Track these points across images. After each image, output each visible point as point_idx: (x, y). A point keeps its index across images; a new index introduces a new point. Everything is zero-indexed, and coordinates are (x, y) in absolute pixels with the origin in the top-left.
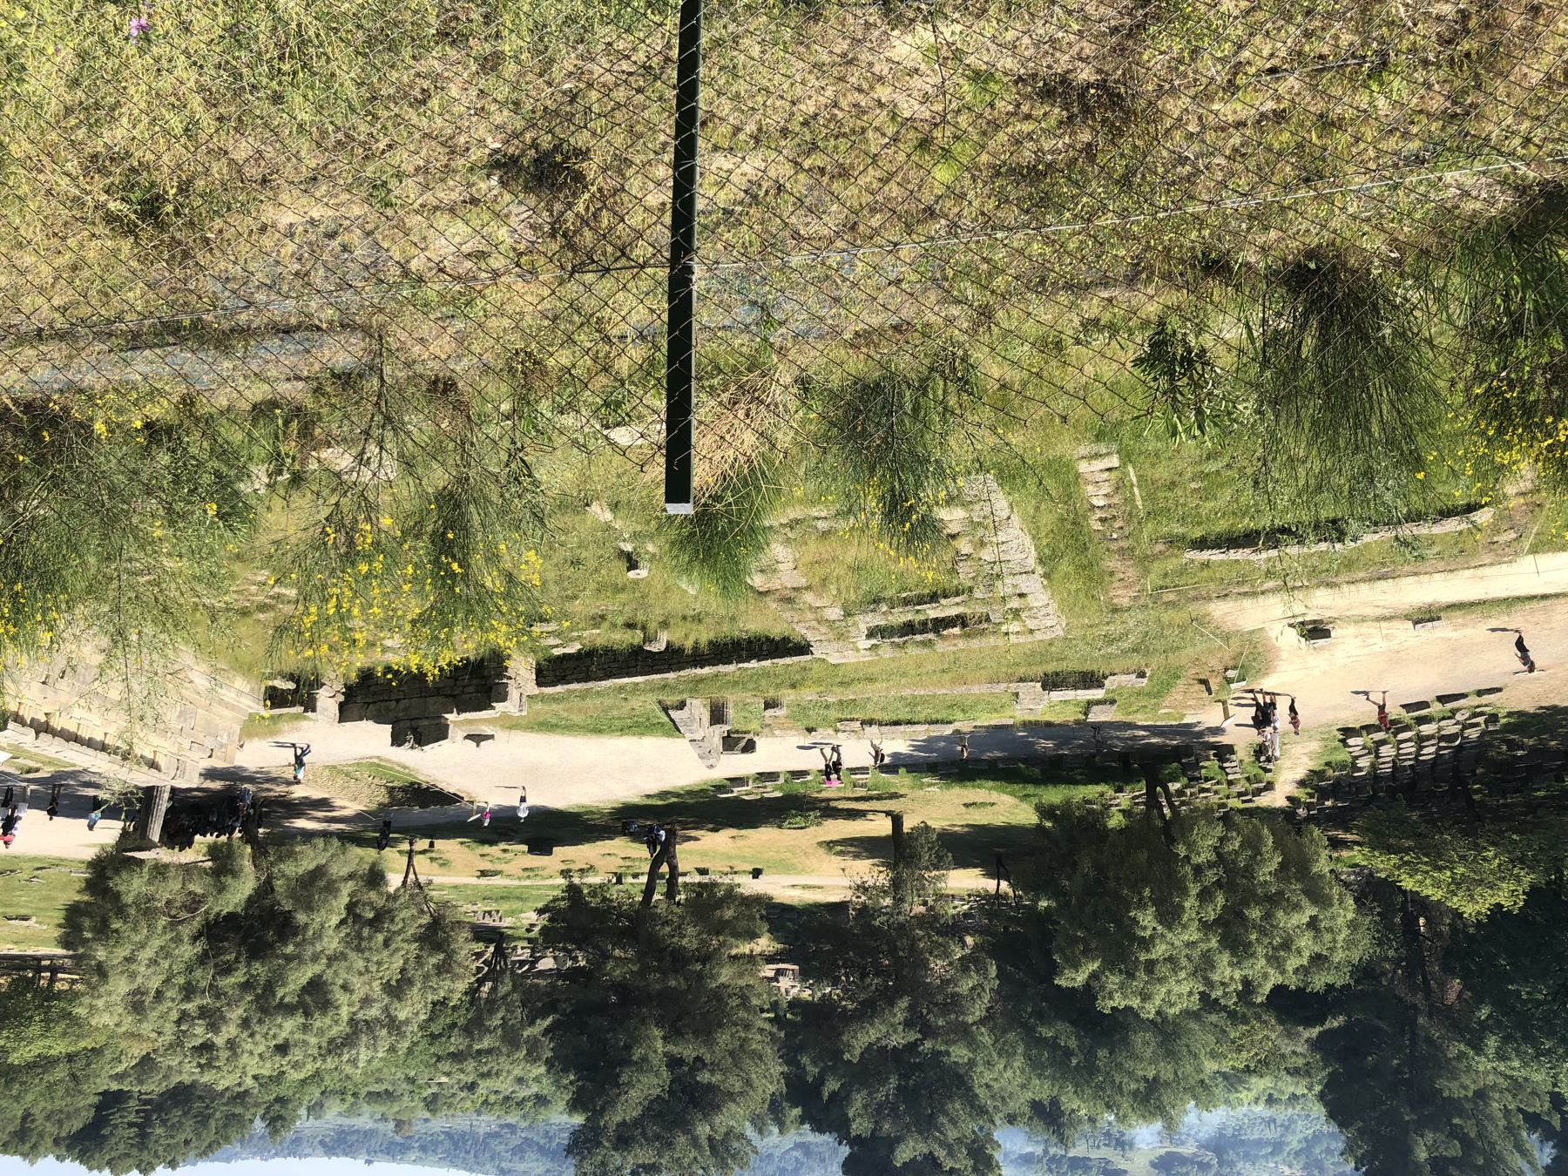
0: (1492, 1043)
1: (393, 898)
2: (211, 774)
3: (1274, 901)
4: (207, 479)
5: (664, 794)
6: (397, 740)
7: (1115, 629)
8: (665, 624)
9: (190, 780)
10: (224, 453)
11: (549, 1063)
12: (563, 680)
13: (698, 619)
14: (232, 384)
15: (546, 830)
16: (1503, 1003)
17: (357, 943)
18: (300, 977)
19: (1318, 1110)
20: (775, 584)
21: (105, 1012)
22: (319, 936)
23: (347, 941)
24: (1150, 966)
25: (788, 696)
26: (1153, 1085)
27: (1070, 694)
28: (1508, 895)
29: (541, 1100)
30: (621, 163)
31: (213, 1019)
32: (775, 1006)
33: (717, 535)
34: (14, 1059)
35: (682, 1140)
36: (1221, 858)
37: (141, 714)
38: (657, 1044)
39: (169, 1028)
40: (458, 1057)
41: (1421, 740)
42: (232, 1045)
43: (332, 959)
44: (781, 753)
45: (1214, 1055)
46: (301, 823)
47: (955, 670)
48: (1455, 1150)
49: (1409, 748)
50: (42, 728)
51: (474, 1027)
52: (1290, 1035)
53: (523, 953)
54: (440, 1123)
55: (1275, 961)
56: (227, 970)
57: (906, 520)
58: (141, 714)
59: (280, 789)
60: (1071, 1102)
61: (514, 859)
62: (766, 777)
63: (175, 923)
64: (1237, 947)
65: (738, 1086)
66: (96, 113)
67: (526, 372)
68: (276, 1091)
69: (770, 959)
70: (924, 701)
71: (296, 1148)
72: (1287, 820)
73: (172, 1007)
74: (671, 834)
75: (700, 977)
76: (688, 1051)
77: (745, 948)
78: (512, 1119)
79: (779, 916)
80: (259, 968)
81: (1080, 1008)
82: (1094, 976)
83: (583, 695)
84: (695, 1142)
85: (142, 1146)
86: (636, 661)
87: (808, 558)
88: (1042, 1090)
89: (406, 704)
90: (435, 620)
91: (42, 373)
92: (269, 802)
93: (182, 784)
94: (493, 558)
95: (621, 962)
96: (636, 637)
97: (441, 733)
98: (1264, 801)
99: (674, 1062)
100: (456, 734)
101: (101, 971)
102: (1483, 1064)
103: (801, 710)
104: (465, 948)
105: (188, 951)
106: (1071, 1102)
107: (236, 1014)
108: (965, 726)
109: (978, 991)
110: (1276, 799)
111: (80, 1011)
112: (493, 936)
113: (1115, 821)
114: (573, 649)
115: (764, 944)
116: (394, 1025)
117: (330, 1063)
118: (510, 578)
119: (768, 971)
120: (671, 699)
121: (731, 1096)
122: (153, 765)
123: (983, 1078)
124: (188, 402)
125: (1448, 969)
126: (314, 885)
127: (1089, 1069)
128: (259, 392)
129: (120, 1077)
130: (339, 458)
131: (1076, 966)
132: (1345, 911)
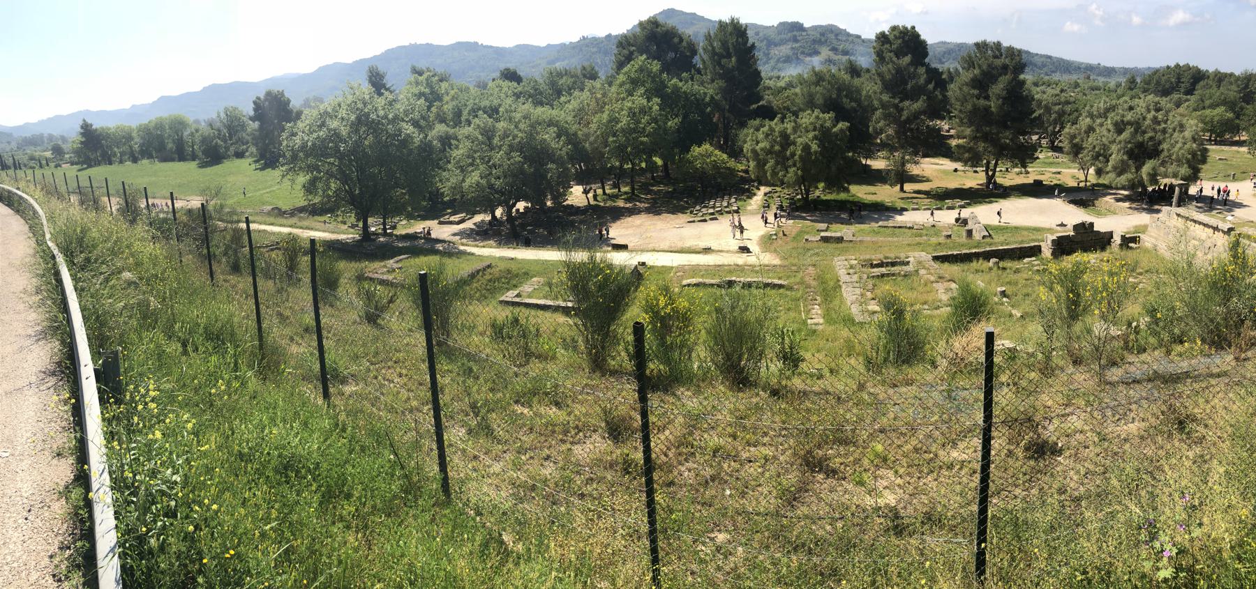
0: (708, 99)
1: (1092, 164)
2: (1158, 211)
3: (769, 152)
4: (1161, 324)
5: (991, 202)
6: (1092, 225)
7: (815, 258)
8: (991, 269)
9: (1165, 209)
10: (1155, 334)
11: (1033, 99)
12: (1031, 248)
13: (977, 271)
14: (1153, 361)
15: (1038, 190)
16: (702, 113)
17: (1105, 147)
18: (1125, 135)
19: (763, 74)
20: (946, 284)
21: (1193, 124)
22: (1119, 150)
23: (1109, 148)
24: (815, 130)
25: (942, 240)
26: (817, 83)
27: (833, 235)
28: (696, 150)
29: (1036, 84)
30: (1010, 454)
31: (1156, 121)
32: (950, 118)
33: (971, 308)
34: (1223, 108)
35: (985, 67)
36: (786, 169)
37: (1183, 235)
38: (994, 105)
39: (1171, 118)
40: (1068, 103)
41: (714, 207)
42: (1149, 111)
43: (1114, 141)
44: (946, 217)
45: (796, 94)
46: (1126, 193)
47: (877, 247)
48: (724, 61)
49: (718, 204)
50: (1216, 229)
51: (1062, 114)
52: (769, 102)
53: (1044, 142)
54: (1074, 77)
55: (772, 130)
56: (1151, 138)
57: (895, 309)
58: (1183, 235)
59: (1134, 206)
60: (846, 77)
61: (1048, 179)
62: (952, 208)
63: (1170, 156)
64: (784, 135)
65: (965, 88)
66: (1201, 460)
67: (1047, 370)
68: (1133, 93)
69: (951, 136)
70: (889, 235)
71: (1125, 71)
72: (761, 182)
73: (1170, 126)
74: (988, 186)
75: (977, 131)
76: (982, 102)
77: (961, 141)
78: (1047, 78)
79: (948, 153)
80: (1140, 139)
81: (841, 113)
82: (835, 126)
83: (1022, 242)
84: (980, 66)
85: (1179, 74)
86: (1002, 255)
87: (936, 293)
88: (857, 81)
89: (1088, 239)
90: (1079, 271)
91: (1218, 361)
92: (1138, 201)
93: (1168, 208)
94: (1058, 297)
95: (1006, 138)
96: (1001, 264)
97: (1076, 227)
98: (768, 189)
99: (987, 98)
100: (1070, 227)
101: (1194, 140)
102: (711, 92)
103: (936, 235)
104: (1065, 145)
105: (1165, 146)
106: (846, 77)
107: (1148, 122)
108: (874, 225)
109: (877, 122)
110: (764, 189)
111: (1201, 125)
112: (1055, 149)
113: (821, 185)
114: (1027, 260)
115: (954, 142)
116: (1091, 116)
117: (1114, 102)
118: (1051, 289)
119: (952, 132)
120: (988, 240)
121: (967, 84)
122: (1178, 215)
123: (878, 87)
124: (1168, 353)
125: (716, 125)
126: (1120, 170)
127: (839, 90)
128: (1144, 357)
129: (1187, 100)
130: (1115, 331)
131: (841, 130)
132: (747, 147)
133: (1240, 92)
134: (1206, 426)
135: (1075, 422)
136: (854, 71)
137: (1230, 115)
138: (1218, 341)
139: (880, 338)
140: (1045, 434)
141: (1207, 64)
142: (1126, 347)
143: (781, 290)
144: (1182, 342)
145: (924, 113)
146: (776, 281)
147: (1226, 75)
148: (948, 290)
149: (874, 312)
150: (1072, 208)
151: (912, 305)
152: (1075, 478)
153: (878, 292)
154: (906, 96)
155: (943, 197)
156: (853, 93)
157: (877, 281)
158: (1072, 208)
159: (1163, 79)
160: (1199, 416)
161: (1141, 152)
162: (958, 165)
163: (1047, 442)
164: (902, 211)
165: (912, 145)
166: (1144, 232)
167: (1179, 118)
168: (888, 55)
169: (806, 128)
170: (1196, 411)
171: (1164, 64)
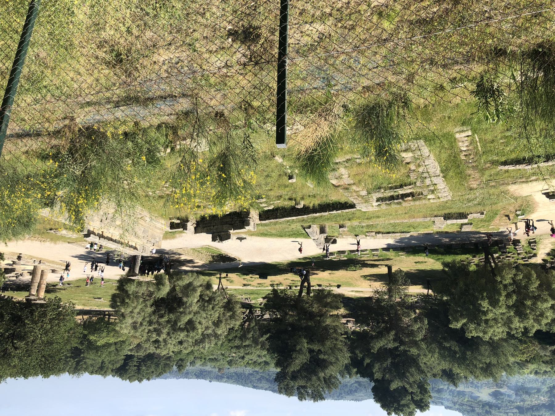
1: (215, 293)
3: (536, 298)
6: (214, 239)
7: (471, 196)
8: (302, 198)
9: (147, 254)
12: (268, 218)
13: (314, 196)
15: (264, 270)
21: (125, 329)
22: (191, 305)
23: (200, 307)
24: (486, 321)
25: (348, 223)
27: (455, 221)
29: (266, 363)
31: (158, 332)
33: (315, 162)
34: (99, 344)
35: (314, 378)
36: (514, 282)
39: (145, 335)
40: (238, 347)
42: (165, 341)
43: (195, 313)
44: (344, 244)
45: (513, 355)
46: (184, 268)
47: (409, 213)
50: (101, 236)
51: (243, 337)
52: (545, 349)
53: (258, 313)
54: (233, 370)
56: (162, 316)
57: (386, 156)
59: (177, 257)
61: (255, 280)
64: (521, 314)
65: (333, 360)
69: (344, 317)
70: (399, 225)
71: (187, 375)
74: (308, 272)
75: (319, 322)
76: (316, 347)
77: (335, 312)
79: (347, 301)
80: (172, 316)
81: (459, 336)
82: (464, 324)
83: (275, 224)
84: (319, 379)
86: (293, 211)
88: (445, 365)
90: (220, 198)
92: (173, 261)
93: (145, 255)
95: (292, 316)
96: (293, 203)
97: (228, 237)
98: (533, 261)
99: (311, 351)
100: (233, 237)
101: (123, 316)
103: (353, 229)
104: (239, 310)
105: (149, 310)
106: (456, 370)
107: (165, 331)
108: (415, 234)
109: (420, 330)
110: (538, 260)
111: (117, 328)
112: (249, 306)
113: (472, 268)
114: (271, 208)
116: (216, 336)
117: (196, 348)
119: (344, 321)
120: (306, 225)
121: (331, 363)
122: (135, 248)
126: (189, 288)
129: (131, 350)
131: (457, 321)
133: (84, 358)
134: (97, 58)
135: (217, 61)
136: (450, 376)
137: (92, 338)
138: (92, 135)
139: (398, 126)
140: (243, 49)
141: (113, 382)
142: (174, 129)
143: (503, 159)
144: (126, 134)
145: (372, 338)
146: (510, 168)
147: (96, 372)
148: (339, 178)
149: (406, 151)
150: (232, 254)
151: (371, 161)
152: (214, 10)
153: (403, 171)
154: (392, 352)
155: (350, 262)
156: (451, 355)
157: (407, 181)
158: (232, 254)
159: (152, 369)
160: (104, 67)
161: (171, 304)
162: (336, 291)
163: (242, 42)
164: (388, 248)
165: (382, 308)
166: (167, 233)
167: (138, 334)
168: (415, 389)
169: (496, 321)
170: (107, 71)
171: (152, 381)
